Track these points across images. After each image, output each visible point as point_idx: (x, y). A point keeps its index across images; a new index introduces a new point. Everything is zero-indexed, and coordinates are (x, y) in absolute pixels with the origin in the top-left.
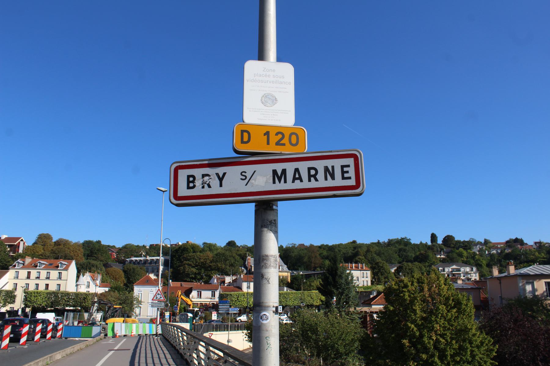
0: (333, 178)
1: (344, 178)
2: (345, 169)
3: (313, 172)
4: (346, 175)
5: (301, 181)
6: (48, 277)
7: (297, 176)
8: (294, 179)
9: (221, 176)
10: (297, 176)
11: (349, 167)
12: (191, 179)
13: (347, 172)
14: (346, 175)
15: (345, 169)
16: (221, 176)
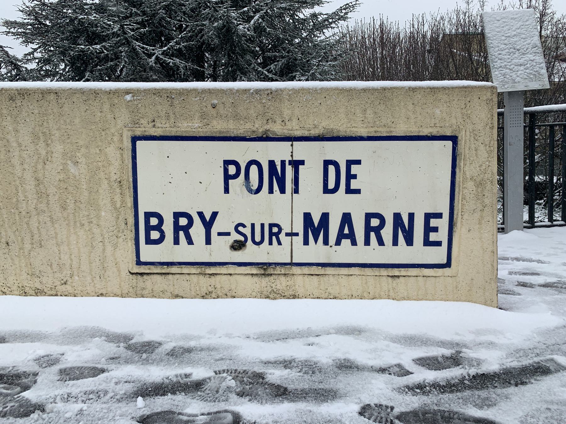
0: (409, 241)
1: (427, 242)
2: (433, 222)
3: (154, 221)
4: (433, 237)
5: (354, 243)
6: (501, 117)
7: (346, 231)
8: (341, 236)
9: (208, 218)
10: (346, 231)
11: (254, 224)
12: (154, 221)
13: (436, 229)
14: (433, 237)
15: (433, 222)
16: (208, 218)
